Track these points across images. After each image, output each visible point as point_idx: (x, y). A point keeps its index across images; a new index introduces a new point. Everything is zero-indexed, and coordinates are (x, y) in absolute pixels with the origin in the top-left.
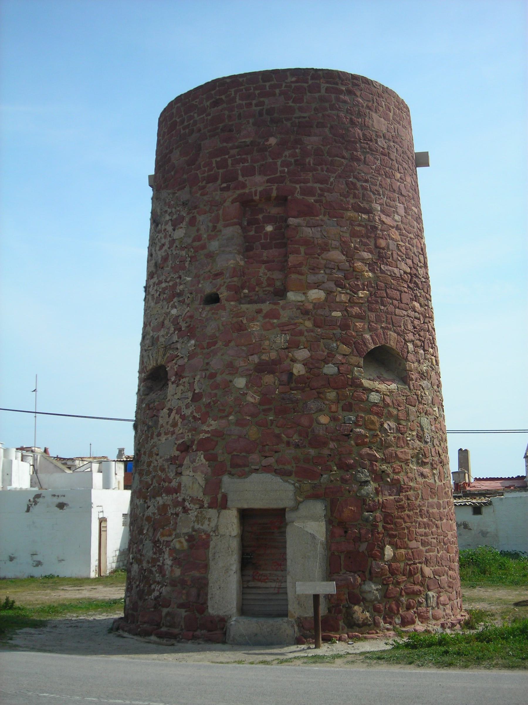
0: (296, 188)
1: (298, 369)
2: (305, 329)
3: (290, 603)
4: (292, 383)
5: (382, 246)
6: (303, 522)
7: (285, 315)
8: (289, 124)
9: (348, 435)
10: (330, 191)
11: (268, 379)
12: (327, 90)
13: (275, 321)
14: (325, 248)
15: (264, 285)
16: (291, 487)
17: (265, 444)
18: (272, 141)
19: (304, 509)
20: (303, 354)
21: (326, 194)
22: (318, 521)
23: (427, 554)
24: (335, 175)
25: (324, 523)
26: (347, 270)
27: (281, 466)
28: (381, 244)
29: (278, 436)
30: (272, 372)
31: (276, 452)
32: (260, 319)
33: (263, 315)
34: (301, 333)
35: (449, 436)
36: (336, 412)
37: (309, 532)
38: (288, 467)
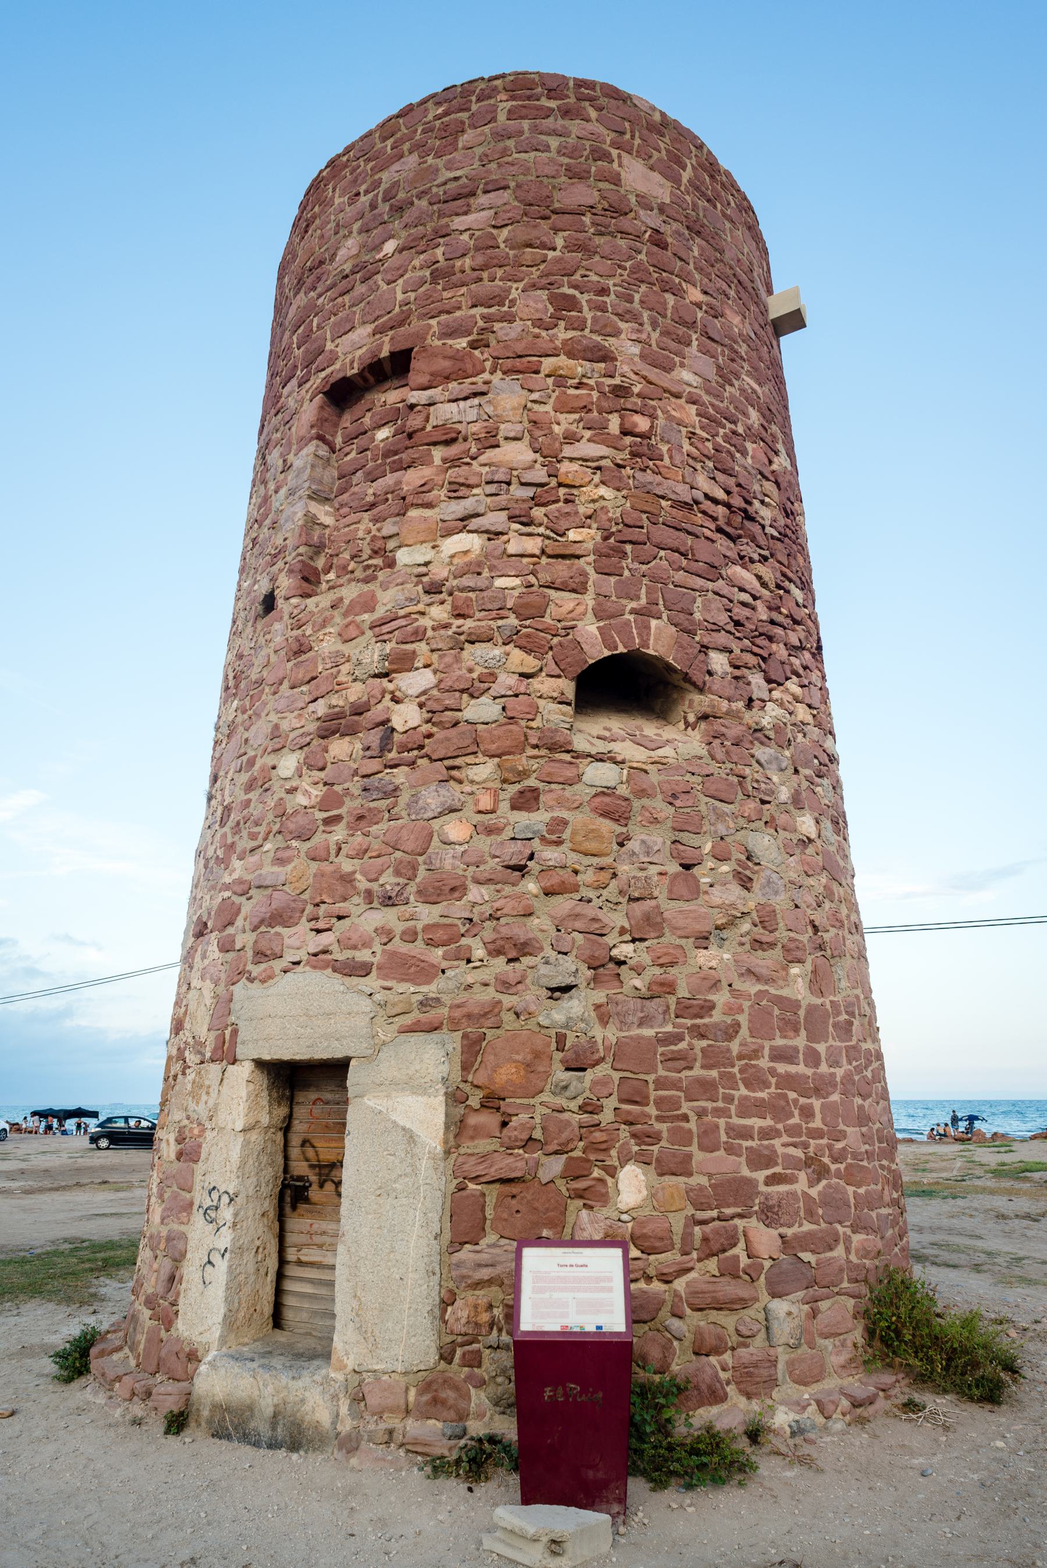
0: (430, 326)
1: (406, 717)
2: (432, 623)
3: (338, 1324)
4: (390, 751)
5: (637, 430)
6: (388, 1096)
7: (388, 599)
8: (424, 203)
9: (520, 868)
10: (509, 318)
11: (340, 748)
12: (511, 115)
13: (366, 616)
14: (490, 440)
15: (365, 556)
16: (366, 1005)
17: (318, 900)
18: (390, 247)
19: (388, 1067)
20: (417, 681)
21: (497, 326)
22: (425, 1093)
23: (770, 1189)
24: (521, 285)
25: (442, 1098)
26: (542, 485)
27: (349, 954)
28: (636, 425)
29: (347, 879)
30: (351, 732)
31: (340, 918)
32: (338, 619)
33: (343, 610)
34: (419, 635)
35: (871, 941)
36: (492, 812)
37: (401, 1123)
38: (363, 955)
